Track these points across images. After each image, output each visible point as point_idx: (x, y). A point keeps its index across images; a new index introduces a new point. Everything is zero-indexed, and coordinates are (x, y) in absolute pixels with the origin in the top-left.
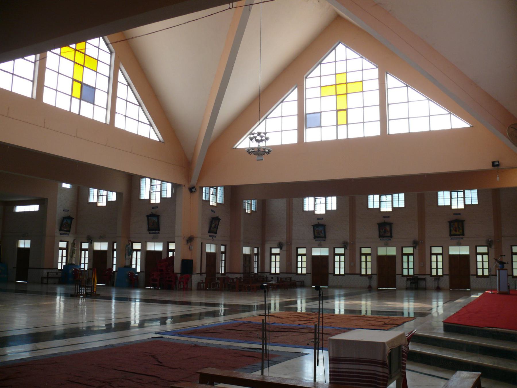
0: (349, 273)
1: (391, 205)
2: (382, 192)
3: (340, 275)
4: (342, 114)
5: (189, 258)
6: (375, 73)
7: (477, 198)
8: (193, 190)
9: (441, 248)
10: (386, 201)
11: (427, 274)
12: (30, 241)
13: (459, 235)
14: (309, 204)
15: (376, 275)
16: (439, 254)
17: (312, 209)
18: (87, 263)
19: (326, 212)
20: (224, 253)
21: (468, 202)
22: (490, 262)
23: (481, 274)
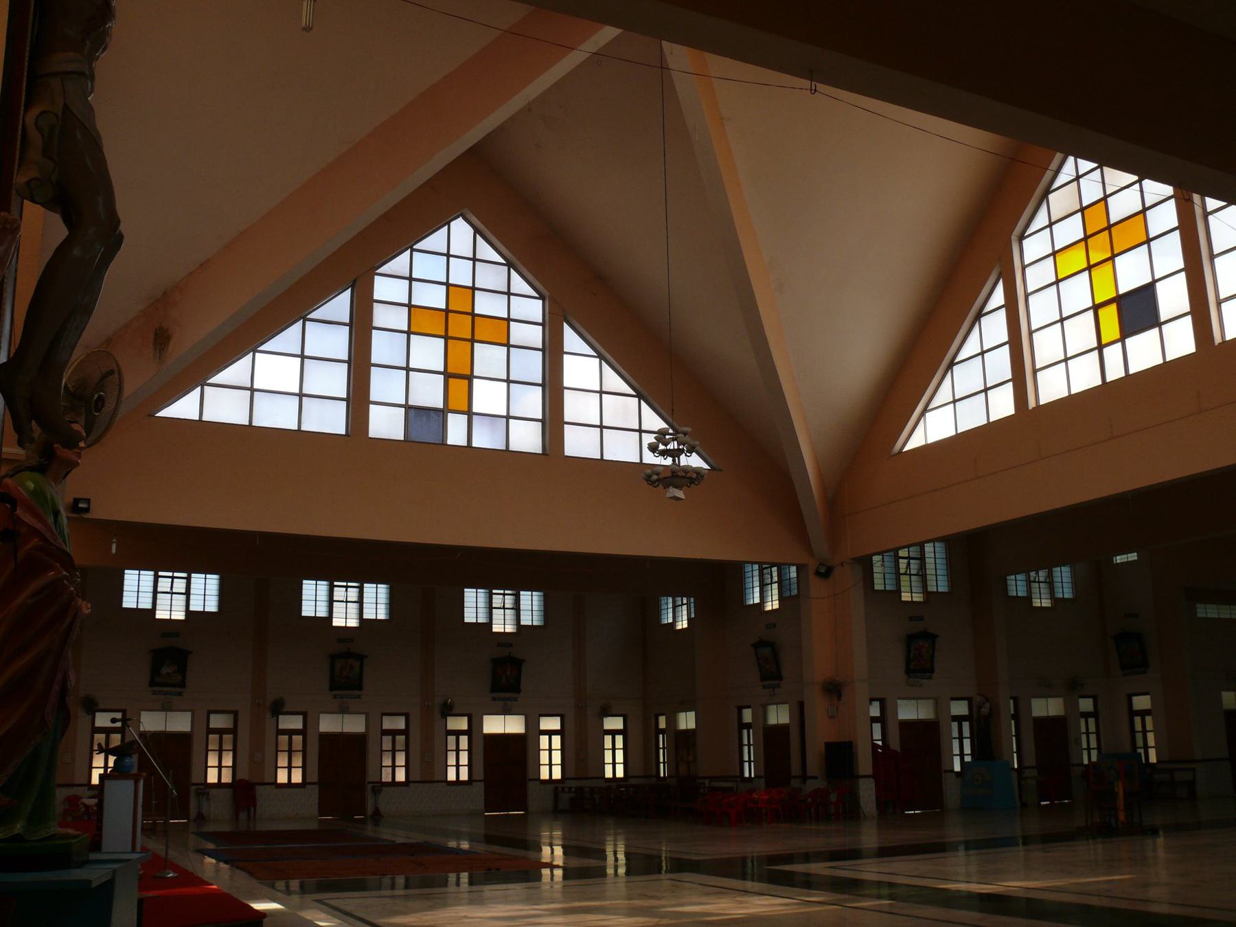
0: (418, 779)
1: (365, 610)
2: (488, 583)
3: (458, 782)
4: (458, 385)
5: (847, 740)
6: (533, 309)
7: (303, 598)
8: (823, 570)
9: (300, 718)
10: (347, 602)
11: (266, 781)
12: (693, 713)
13: (173, 685)
14: (474, 604)
15: (531, 777)
16: (296, 732)
17: (322, 612)
18: (870, 771)
19: (186, 615)
20: (1095, 714)
21: (196, 606)
22: (274, 749)
23: (215, 780)
